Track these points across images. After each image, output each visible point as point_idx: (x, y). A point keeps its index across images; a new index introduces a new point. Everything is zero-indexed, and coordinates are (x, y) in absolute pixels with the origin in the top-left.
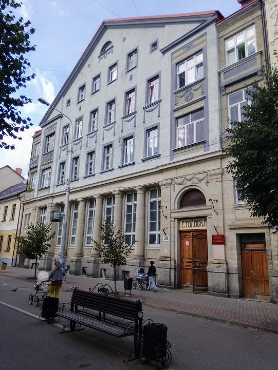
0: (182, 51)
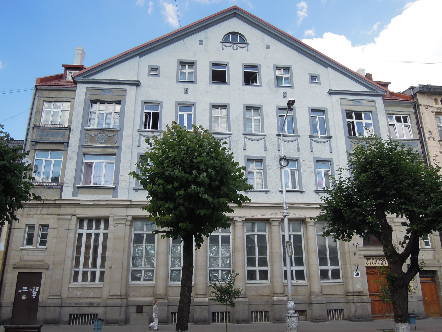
0: (351, 102)
